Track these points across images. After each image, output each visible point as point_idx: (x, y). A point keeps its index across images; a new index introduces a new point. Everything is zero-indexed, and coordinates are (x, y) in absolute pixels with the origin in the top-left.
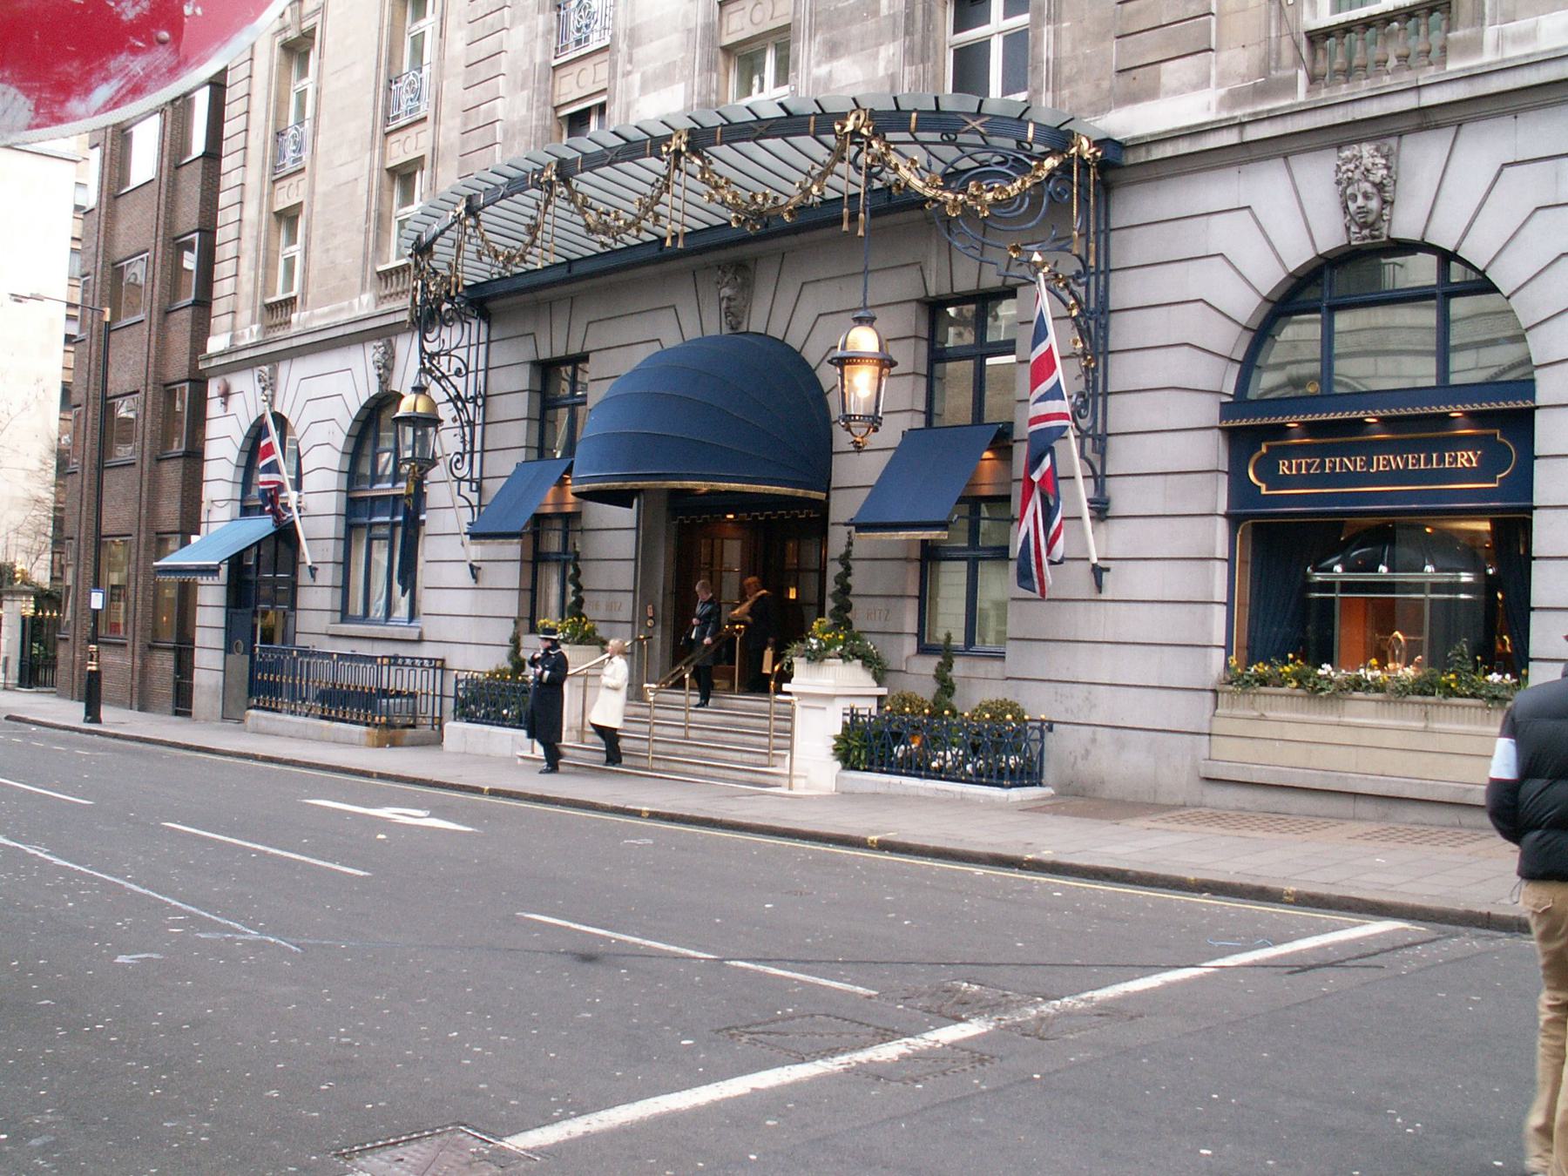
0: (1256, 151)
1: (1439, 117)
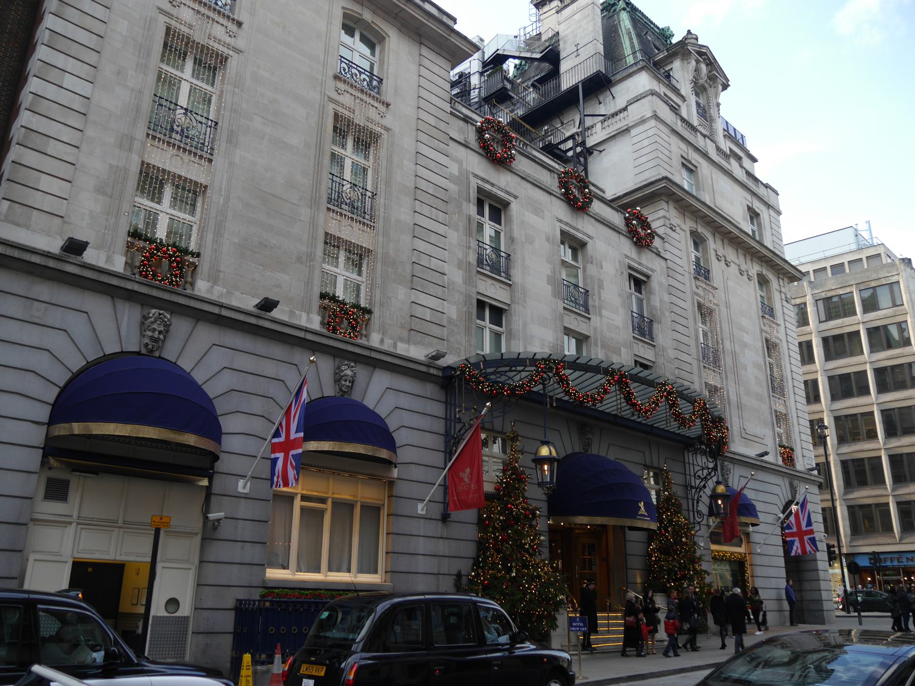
0: (808, 481)
1: (734, 461)
